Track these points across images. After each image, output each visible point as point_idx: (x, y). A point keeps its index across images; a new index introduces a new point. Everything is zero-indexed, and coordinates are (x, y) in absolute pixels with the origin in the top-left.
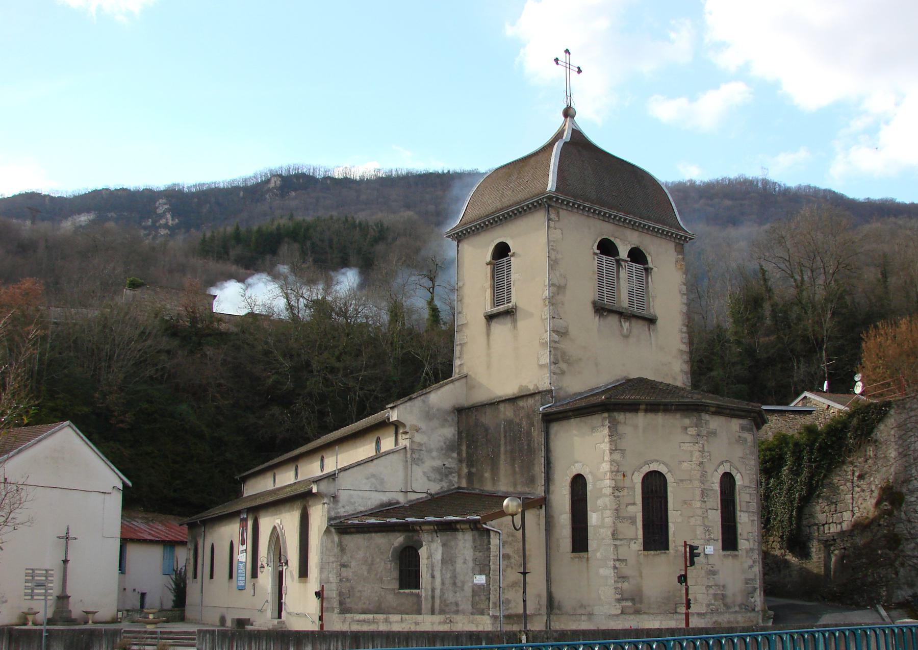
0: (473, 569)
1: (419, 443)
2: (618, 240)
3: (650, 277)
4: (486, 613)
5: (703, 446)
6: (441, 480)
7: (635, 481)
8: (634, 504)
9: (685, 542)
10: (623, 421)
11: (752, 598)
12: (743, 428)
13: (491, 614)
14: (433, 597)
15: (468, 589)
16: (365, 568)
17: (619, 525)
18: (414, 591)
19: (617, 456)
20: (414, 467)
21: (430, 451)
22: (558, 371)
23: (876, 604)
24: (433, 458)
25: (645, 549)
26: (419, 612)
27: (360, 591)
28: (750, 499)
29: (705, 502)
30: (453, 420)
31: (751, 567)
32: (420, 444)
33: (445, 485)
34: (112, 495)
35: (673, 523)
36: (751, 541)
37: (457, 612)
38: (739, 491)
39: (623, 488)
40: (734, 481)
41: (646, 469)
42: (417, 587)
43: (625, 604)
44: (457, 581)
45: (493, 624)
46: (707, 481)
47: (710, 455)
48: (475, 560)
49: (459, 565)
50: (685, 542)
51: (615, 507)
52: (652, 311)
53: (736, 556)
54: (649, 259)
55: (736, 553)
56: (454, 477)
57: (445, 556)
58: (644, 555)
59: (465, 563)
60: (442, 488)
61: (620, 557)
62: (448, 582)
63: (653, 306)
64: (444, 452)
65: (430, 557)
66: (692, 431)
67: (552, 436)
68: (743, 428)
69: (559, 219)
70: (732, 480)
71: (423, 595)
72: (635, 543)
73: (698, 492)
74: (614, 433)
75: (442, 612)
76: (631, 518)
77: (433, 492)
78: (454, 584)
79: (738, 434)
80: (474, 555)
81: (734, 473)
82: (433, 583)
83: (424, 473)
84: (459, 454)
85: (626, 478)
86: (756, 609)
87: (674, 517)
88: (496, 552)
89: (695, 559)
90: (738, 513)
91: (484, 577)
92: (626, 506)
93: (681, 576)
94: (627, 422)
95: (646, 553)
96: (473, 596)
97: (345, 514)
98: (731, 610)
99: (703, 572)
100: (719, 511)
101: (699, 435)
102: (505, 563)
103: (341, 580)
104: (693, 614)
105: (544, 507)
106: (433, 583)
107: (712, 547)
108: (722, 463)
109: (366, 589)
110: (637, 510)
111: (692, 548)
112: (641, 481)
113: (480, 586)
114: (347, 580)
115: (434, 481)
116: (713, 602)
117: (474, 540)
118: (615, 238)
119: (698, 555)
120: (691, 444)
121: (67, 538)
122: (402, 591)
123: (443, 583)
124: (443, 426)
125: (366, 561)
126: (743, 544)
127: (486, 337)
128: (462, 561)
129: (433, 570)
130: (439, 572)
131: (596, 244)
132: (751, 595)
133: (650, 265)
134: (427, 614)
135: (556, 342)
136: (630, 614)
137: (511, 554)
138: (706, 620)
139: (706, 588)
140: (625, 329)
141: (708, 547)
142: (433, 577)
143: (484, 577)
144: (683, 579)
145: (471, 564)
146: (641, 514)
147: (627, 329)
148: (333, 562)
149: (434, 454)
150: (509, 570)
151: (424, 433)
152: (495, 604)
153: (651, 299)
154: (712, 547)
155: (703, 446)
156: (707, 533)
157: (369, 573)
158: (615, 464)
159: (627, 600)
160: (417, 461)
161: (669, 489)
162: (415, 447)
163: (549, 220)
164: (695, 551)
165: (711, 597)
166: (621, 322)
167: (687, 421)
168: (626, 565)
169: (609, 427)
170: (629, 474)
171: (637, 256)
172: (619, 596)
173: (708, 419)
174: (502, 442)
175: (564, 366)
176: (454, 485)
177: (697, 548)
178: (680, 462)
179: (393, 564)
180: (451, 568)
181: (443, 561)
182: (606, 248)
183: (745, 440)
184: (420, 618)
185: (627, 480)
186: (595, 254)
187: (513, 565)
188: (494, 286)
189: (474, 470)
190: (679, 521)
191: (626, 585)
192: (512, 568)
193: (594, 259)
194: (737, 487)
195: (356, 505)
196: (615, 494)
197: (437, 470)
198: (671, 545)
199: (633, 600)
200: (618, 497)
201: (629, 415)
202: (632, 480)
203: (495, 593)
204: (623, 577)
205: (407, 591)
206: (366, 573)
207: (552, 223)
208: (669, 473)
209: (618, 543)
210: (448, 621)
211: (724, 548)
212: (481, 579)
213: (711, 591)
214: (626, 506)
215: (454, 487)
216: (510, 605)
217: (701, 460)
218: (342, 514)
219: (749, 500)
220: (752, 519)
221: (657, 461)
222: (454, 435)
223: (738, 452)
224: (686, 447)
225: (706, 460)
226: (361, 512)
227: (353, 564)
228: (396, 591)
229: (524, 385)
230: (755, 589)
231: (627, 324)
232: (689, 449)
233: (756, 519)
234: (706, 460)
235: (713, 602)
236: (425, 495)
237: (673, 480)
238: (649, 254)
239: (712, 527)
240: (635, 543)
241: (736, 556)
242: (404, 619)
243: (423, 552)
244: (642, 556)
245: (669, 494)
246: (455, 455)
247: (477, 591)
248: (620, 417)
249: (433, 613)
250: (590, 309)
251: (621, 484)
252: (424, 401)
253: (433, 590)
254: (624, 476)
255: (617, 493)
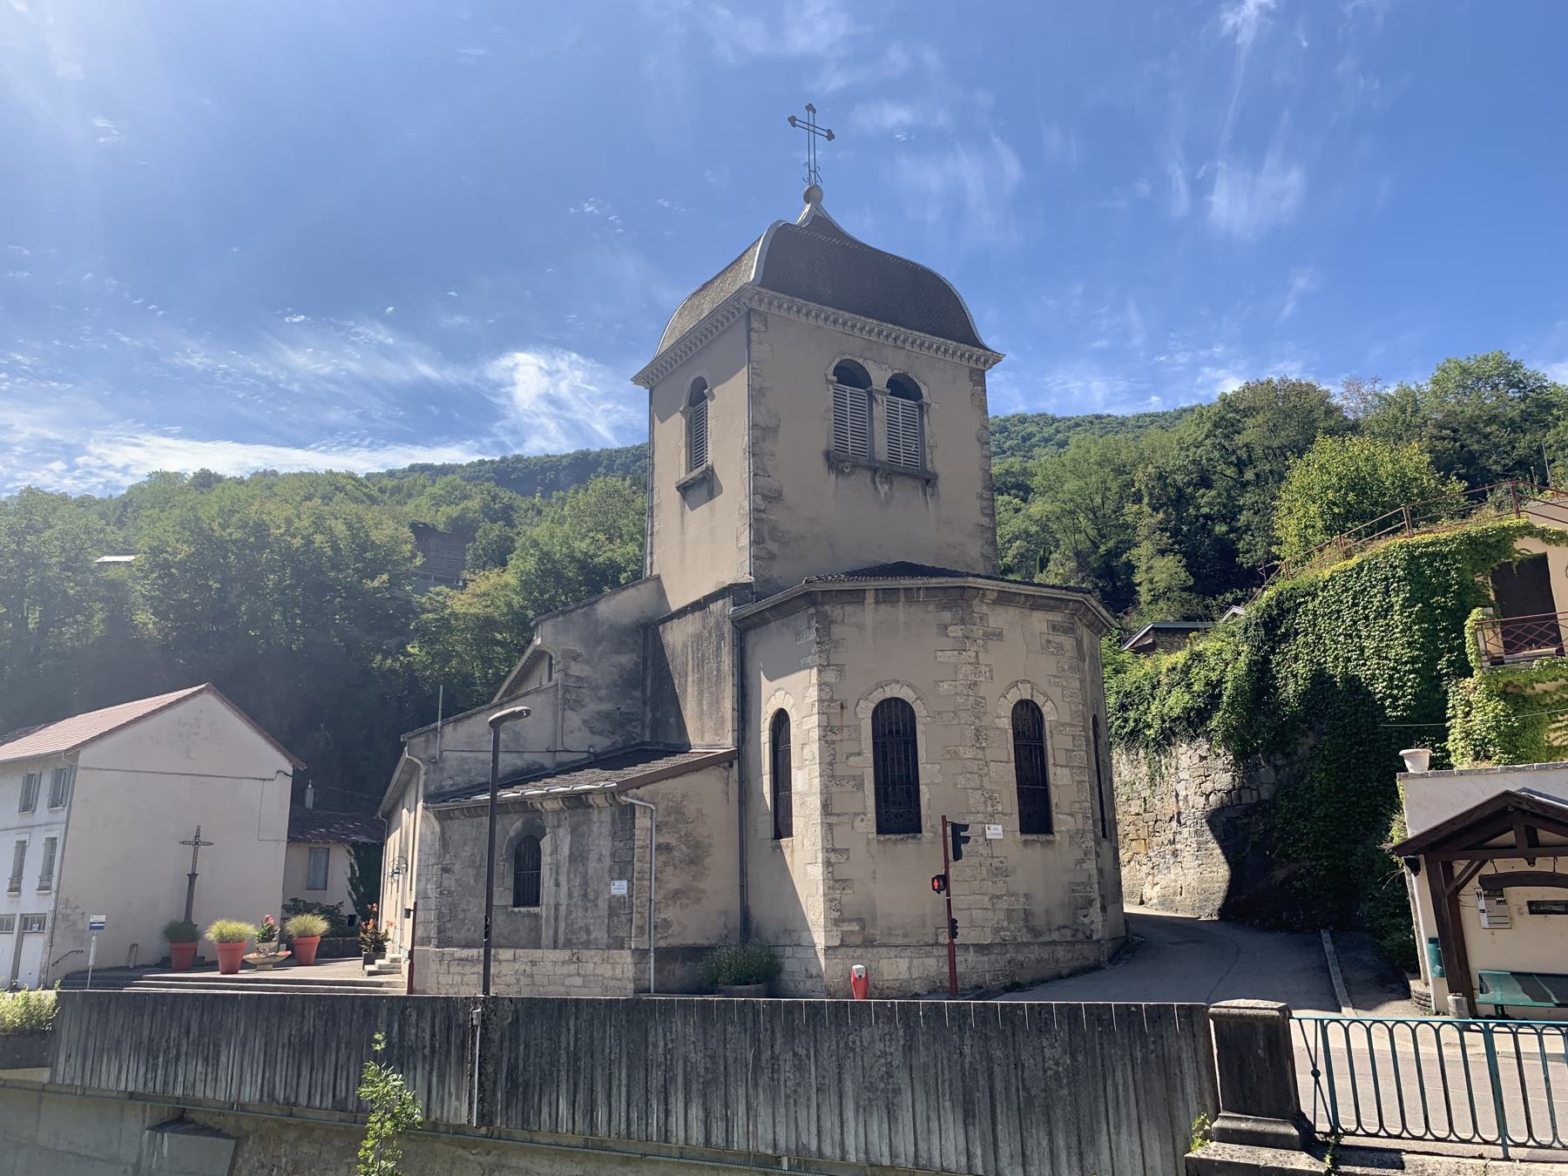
0: (611, 870)
1: (577, 677)
2: (870, 362)
3: (925, 418)
4: (626, 946)
5: (977, 654)
6: (613, 733)
7: (861, 715)
8: (860, 754)
9: (944, 818)
10: (839, 619)
11: (1085, 916)
12: (1054, 628)
13: (633, 946)
14: (556, 918)
15: (603, 904)
16: (471, 872)
17: (834, 789)
18: (531, 909)
19: (831, 676)
20: (569, 713)
21: (594, 689)
22: (762, 554)
23: (1320, 928)
24: (601, 700)
25: (880, 831)
26: (537, 945)
27: (464, 911)
28: (1074, 745)
29: (984, 748)
30: (635, 642)
31: (1081, 862)
32: (578, 678)
33: (619, 739)
34: (275, 782)
35: (926, 784)
36: (1079, 817)
37: (587, 945)
38: (1051, 732)
39: (841, 728)
40: (1041, 715)
41: (879, 696)
42: (537, 903)
43: (846, 927)
44: (589, 890)
45: (636, 964)
46: (985, 713)
47: (991, 670)
48: (613, 855)
49: (592, 865)
50: (944, 818)
51: (829, 759)
52: (929, 466)
53: (1049, 842)
54: (924, 390)
55: (1050, 837)
56: (636, 727)
57: (574, 850)
58: (878, 841)
59: (600, 859)
60: (613, 744)
61: (837, 846)
62: (576, 892)
63: (932, 461)
64: (618, 689)
65: (555, 851)
66: (955, 631)
67: (749, 647)
68: (1054, 628)
69: (767, 328)
70: (1037, 712)
71: (544, 915)
72: (862, 820)
73: (969, 732)
74: (826, 641)
75: (568, 944)
76: (854, 778)
77: (598, 750)
78: (585, 895)
79: (1045, 637)
80: (613, 846)
81: (1039, 700)
82: (557, 895)
83: (584, 722)
84: (644, 692)
85: (845, 711)
86: (1095, 938)
87: (928, 772)
88: (643, 840)
89: (963, 847)
90: (1051, 769)
91: (625, 883)
92: (847, 758)
93: (938, 877)
94: (846, 621)
95: (882, 838)
96: (610, 916)
97: (453, 789)
98: (1042, 939)
99: (984, 870)
100: (1012, 765)
101: (967, 638)
102: (662, 858)
103: (441, 893)
104: (966, 947)
105: (736, 764)
106: (557, 895)
107: (1000, 827)
108: (1015, 684)
109: (471, 907)
110: (864, 765)
111: (958, 829)
112: (870, 715)
113: (619, 899)
114: (449, 892)
115: (600, 734)
116: (1005, 924)
117: (613, 821)
118: (865, 359)
119: (967, 839)
120: (956, 653)
121: (197, 843)
122: (516, 909)
123: (570, 896)
124: (619, 652)
125: (473, 861)
126: (1063, 821)
127: (679, 516)
128: (597, 857)
129: (557, 873)
130: (566, 877)
131: (832, 368)
132: (1083, 912)
133: (926, 398)
134: (548, 948)
135: (759, 511)
136: (857, 946)
137: (674, 842)
138: (993, 957)
139: (990, 899)
140: (883, 494)
141: (992, 827)
142: (557, 885)
143: (625, 883)
144: (943, 882)
145: (608, 862)
146: (871, 770)
147: (885, 494)
148: (433, 865)
149: (603, 692)
150: (669, 869)
151: (587, 662)
152: (641, 928)
153: (927, 450)
154: (1000, 827)
155: (977, 654)
156: (989, 802)
157: (476, 880)
158: (827, 689)
159: (850, 921)
160: (576, 705)
161: (919, 728)
162: (571, 682)
163: (749, 330)
164: (962, 834)
165: (1001, 915)
166: (874, 483)
167: (947, 616)
168: (847, 859)
169: (817, 629)
170: (850, 705)
171: (902, 387)
172: (836, 915)
173: (985, 612)
174: (690, 668)
175: (773, 546)
176: (634, 739)
177: (965, 828)
178: (937, 682)
179: (507, 865)
180: (581, 869)
181: (572, 858)
182: (850, 375)
183: (1060, 647)
184: (538, 953)
185: (849, 712)
186: (828, 381)
187: (677, 862)
188: (691, 444)
189: (658, 715)
190: (937, 781)
191: (847, 897)
192: (675, 867)
193: (828, 390)
194: (1047, 724)
195: (473, 774)
196: (828, 738)
197: (607, 716)
198: (926, 823)
199: (860, 920)
200: (833, 742)
201: (849, 609)
202: (856, 714)
203: (641, 910)
204: (843, 881)
205: (523, 909)
206: (472, 881)
207: (754, 336)
208: (918, 701)
209: (833, 820)
210: (575, 959)
211: (1025, 828)
212: (620, 888)
213: (1004, 904)
214: (847, 758)
215: (634, 743)
216: (670, 931)
217: (972, 677)
218: (447, 789)
219: (1071, 747)
220: (1078, 778)
221: (898, 682)
222: (636, 664)
223: (1047, 665)
224: (943, 657)
225: (982, 679)
226: (480, 784)
227: (457, 868)
228: (510, 909)
229: (721, 580)
230: (1090, 902)
231: (886, 487)
232: (953, 660)
233: (1086, 778)
234: (982, 679)
235: (1005, 924)
236: (585, 755)
237: (925, 713)
238: (924, 383)
239: (999, 792)
240: (862, 820)
241: (1049, 842)
242: (517, 956)
243: (546, 844)
244: (874, 845)
245: (919, 736)
246: (637, 694)
247: (617, 907)
248: (835, 612)
249: (555, 947)
250: (821, 462)
251: (836, 722)
252: (586, 615)
253: (557, 907)
254: (842, 707)
255: (831, 737)
